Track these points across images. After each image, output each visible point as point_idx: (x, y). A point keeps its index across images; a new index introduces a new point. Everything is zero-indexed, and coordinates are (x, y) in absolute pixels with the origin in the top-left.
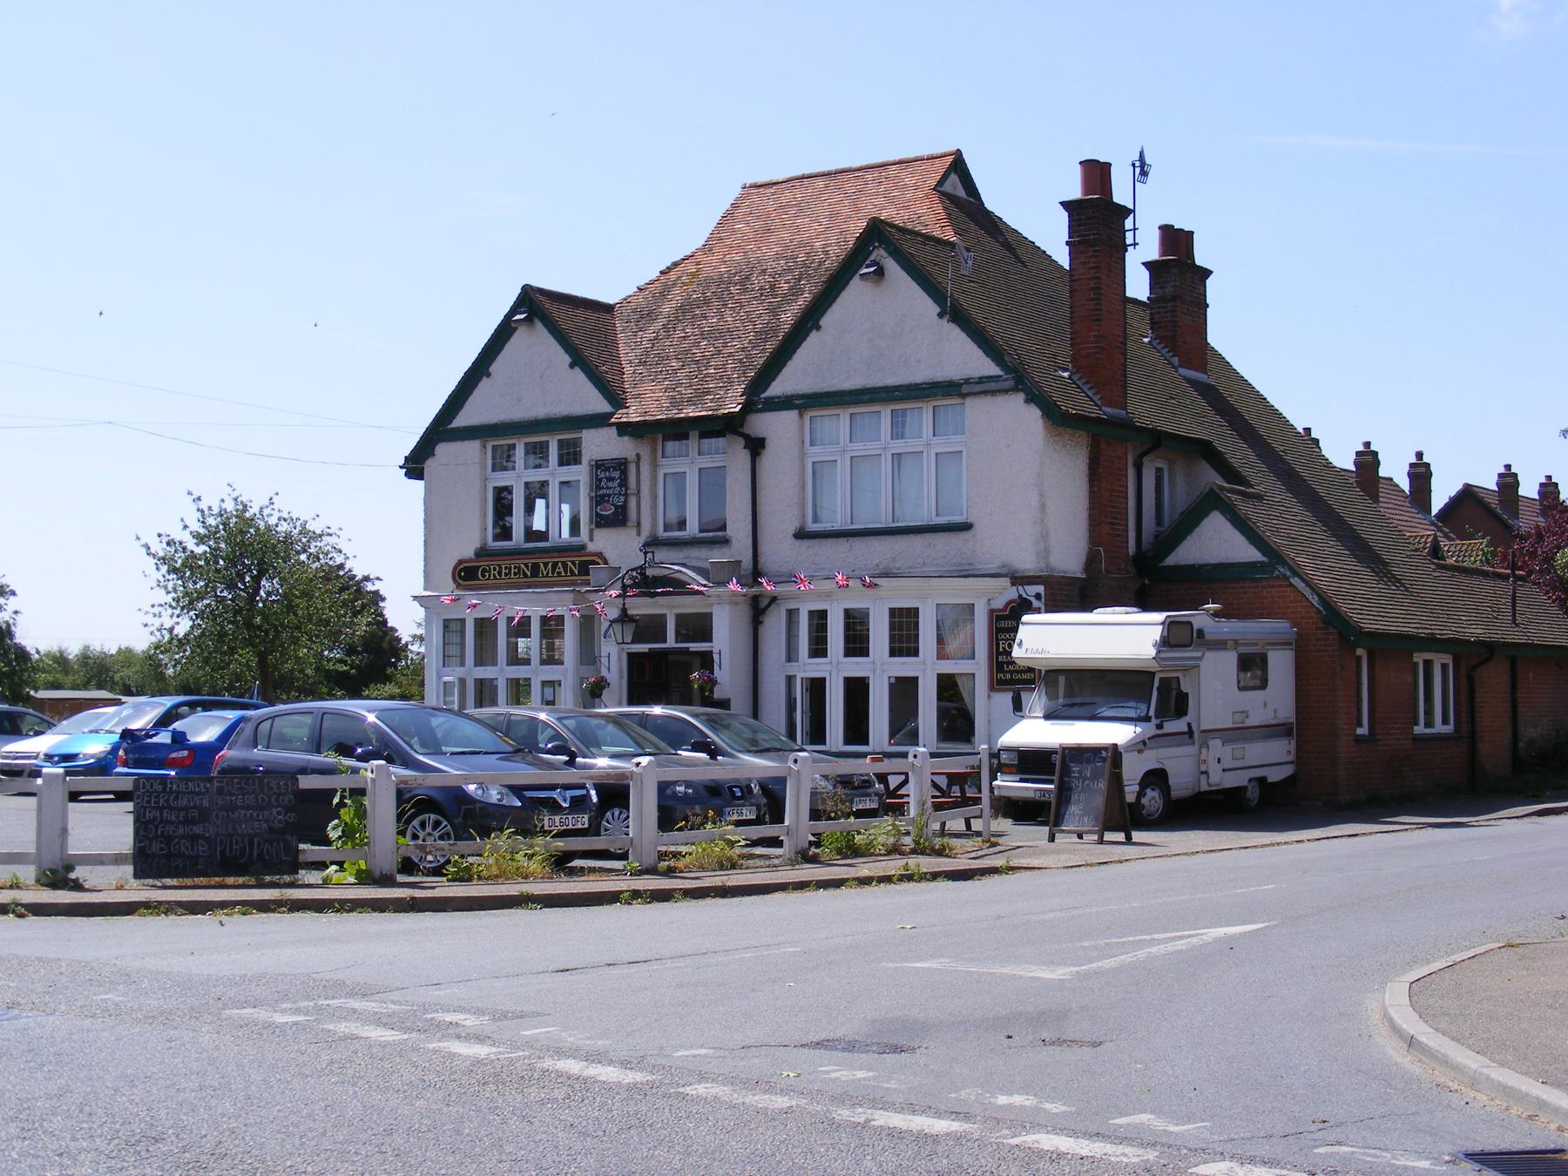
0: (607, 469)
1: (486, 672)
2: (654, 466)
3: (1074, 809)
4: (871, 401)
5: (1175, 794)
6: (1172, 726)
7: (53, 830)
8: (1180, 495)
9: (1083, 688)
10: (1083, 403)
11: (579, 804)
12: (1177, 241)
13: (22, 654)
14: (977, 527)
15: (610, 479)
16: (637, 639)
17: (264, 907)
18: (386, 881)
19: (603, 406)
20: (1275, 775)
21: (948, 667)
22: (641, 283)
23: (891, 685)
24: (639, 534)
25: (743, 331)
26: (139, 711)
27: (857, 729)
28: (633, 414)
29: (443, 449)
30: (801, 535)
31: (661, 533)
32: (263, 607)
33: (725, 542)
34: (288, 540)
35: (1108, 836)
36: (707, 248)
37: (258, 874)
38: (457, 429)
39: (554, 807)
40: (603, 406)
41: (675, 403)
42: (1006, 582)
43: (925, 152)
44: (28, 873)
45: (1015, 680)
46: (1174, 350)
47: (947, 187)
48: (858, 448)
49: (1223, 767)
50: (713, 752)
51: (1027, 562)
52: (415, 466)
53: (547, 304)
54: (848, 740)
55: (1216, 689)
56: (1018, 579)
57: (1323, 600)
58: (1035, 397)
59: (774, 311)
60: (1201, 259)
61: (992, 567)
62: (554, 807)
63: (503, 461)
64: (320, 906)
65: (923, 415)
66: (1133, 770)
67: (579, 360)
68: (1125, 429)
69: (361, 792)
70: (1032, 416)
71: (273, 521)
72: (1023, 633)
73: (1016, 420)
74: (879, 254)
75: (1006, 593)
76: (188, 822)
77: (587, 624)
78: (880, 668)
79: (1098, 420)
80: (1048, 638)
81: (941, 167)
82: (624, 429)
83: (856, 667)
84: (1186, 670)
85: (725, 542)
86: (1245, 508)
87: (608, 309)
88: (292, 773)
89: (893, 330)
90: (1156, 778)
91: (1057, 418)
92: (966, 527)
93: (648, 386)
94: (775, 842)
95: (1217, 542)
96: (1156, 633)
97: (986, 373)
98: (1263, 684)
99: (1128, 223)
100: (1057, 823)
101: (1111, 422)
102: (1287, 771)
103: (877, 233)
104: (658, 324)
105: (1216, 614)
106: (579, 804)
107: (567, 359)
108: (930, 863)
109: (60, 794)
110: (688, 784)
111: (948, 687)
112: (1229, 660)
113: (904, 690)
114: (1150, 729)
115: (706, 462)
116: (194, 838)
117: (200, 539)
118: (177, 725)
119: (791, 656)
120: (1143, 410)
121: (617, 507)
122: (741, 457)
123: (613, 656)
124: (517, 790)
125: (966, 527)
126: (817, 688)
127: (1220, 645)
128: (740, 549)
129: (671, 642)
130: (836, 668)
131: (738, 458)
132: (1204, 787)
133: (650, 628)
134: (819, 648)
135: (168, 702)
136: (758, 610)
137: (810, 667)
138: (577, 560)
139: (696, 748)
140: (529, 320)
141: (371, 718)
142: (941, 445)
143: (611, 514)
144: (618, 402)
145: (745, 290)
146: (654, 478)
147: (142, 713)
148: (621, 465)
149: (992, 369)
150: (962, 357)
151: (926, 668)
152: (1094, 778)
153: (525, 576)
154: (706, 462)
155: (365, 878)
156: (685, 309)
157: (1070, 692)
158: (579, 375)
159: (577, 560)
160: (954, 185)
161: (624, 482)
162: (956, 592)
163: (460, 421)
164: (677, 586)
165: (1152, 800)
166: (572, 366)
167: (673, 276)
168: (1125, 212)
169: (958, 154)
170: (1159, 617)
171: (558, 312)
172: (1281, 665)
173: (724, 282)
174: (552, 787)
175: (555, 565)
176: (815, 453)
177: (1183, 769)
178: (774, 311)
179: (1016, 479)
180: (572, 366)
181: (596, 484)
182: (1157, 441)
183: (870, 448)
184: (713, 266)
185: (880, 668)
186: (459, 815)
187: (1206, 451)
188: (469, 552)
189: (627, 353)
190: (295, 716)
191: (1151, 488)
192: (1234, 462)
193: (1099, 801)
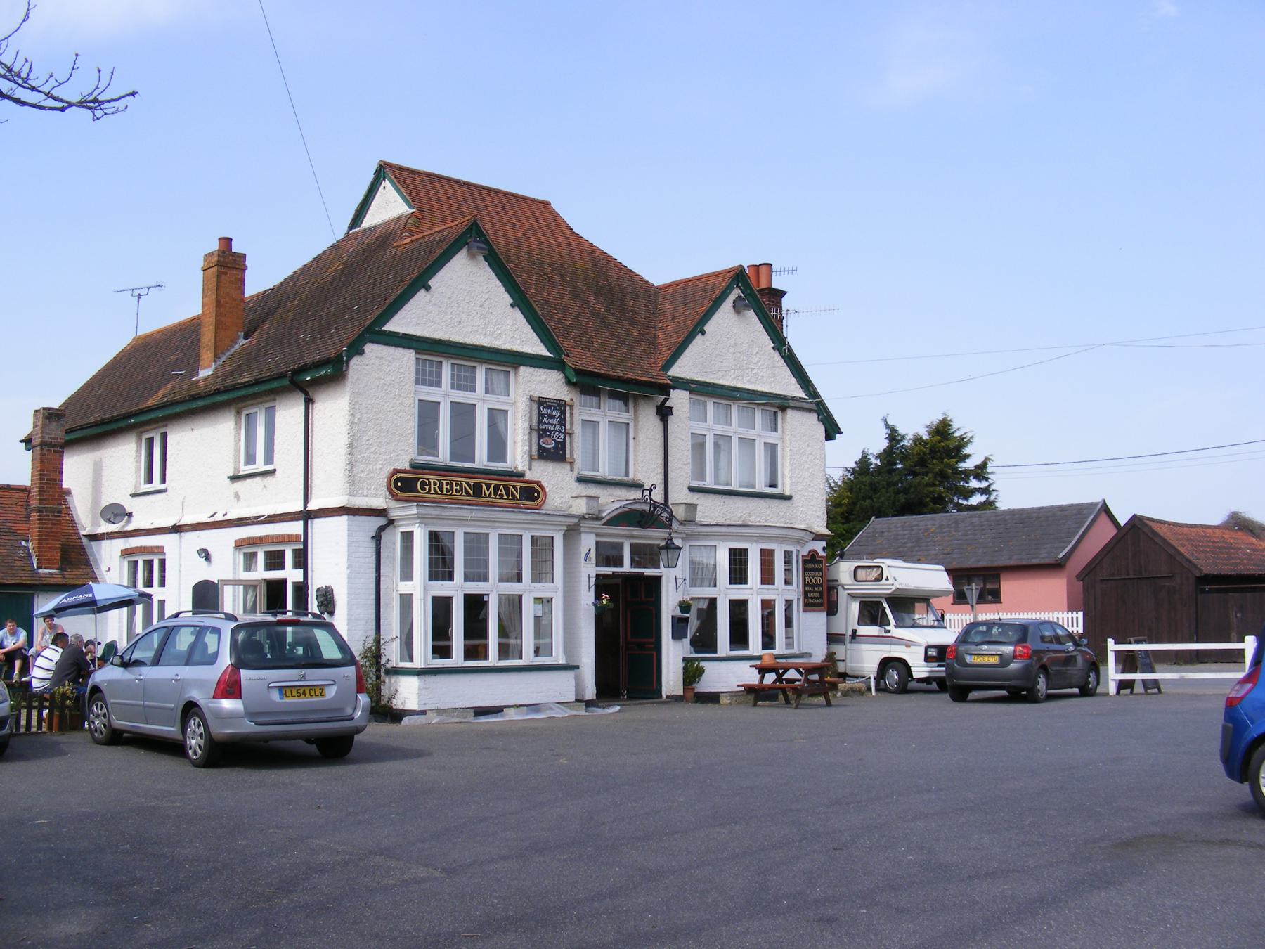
0: (549, 407)
14: (795, 498)
15: (551, 416)
23: (482, 596)
24: (572, 470)
38: (395, 335)
63: (427, 377)
92: (789, 498)
107: (699, 337)
121: (557, 443)
129: (627, 567)
130: (725, 593)
138: (519, 485)
148: (561, 406)
153: (468, 494)
158: (517, 315)
159: (519, 485)
166: (428, 288)
175: (497, 487)
180: (428, 288)
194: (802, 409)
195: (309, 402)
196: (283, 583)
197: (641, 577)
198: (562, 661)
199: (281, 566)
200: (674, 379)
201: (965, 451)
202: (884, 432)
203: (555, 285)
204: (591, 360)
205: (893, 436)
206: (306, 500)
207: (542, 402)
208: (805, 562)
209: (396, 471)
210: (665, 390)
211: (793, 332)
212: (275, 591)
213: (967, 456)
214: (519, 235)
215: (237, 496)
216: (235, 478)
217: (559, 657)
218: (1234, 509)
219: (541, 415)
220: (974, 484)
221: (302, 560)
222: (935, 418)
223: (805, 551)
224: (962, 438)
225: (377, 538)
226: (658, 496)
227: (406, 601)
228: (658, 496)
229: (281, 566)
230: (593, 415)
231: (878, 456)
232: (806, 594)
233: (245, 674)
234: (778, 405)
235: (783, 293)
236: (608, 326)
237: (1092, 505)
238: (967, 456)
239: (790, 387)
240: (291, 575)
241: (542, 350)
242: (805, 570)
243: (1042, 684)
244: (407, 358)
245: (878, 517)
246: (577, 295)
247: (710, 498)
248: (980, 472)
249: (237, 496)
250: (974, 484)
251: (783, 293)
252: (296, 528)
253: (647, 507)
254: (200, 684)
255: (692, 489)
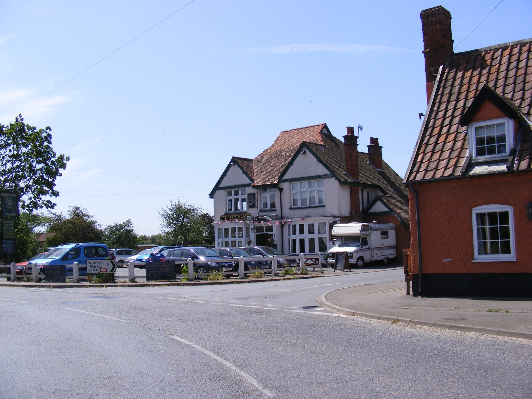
1: (227, 240)
2: (261, 194)
3: (339, 265)
4: (304, 180)
5: (366, 261)
6: (364, 247)
7: (131, 273)
8: (372, 197)
9: (347, 240)
10: (349, 180)
11: (230, 266)
12: (374, 141)
13: (135, 237)
16: (257, 232)
17: (168, 285)
18: (192, 280)
19: (250, 182)
20: (391, 257)
21: (321, 236)
22: (259, 154)
25: (279, 164)
26: (155, 250)
27: (312, 249)
28: (255, 184)
29: (217, 192)
30: (291, 208)
31: (262, 209)
32: (186, 227)
33: (275, 210)
34: (190, 210)
35: (345, 270)
36: (273, 146)
37: (168, 279)
39: (225, 266)
40: (250, 182)
41: (264, 181)
42: (332, 218)
43: (318, 124)
44: (127, 280)
45: (333, 238)
46: (374, 165)
47: (323, 131)
48: (302, 190)
49: (377, 256)
50: (264, 256)
51: (336, 213)
52: (211, 196)
53: (238, 161)
54: (310, 251)
55: (375, 239)
56: (335, 217)
57: (401, 219)
58: (337, 178)
59: (285, 160)
60: (380, 144)
61: (329, 215)
62: (225, 266)
63: (230, 194)
64: (178, 285)
65: (314, 183)
66: (356, 256)
67: (244, 172)
68: (358, 184)
69: (186, 264)
70: (337, 182)
71: (187, 206)
72: (334, 229)
73: (332, 184)
74: (305, 149)
75: (332, 220)
76: (156, 270)
77: (247, 229)
78: (307, 236)
79: (351, 182)
80: (340, 229)
81: (321, 127)
82: (254, 187)
83: (302, 236)
84: (368, 235)
85: (275, 210)
86: (385, 200)
87: (252, 160)
88: (174, 261)
89: (308, 164)
90: (361, 258)
91: (342, 183)
92: (324, 206)
93: (259, 178)
94: (270, 273)
95: (379, 207)
96: (360, 228)
97: (325, 174)
98: (387, 238)
99: (358, 140)
100: (336, 268)
101: (354, 183)
102: (395, 256)
103: (304, 144)
104: (262, 164)
105: (376, 223)
106: (230, 266)
108: (305, 275)
109: (133, 266)
110: (254, 262)
111: (321, 241)
112: (379, 233)
113: (312, 241)
114: (360, 248)
115: (271, 193)
116: (157, 273)
117: (171, 211)
118: (162, 253)
119: (289, 234)
120: (362, 179)
122: (278, 192)
123: (253, 236)
124: (218, 263)
125: (324, 206)
126: (294, 241)
127: (376, 230)
128: (278, 212)
129: (265, 232)
131: (277, 193)
132: (373, 260)
133: (259, 229)
134: (294, 233)
135: (161, 247)
136: (282, 226)
137: (293, 237)
139: (260, 255)
140: (234, 164)
141: (192, 251)
142: (319, 189)
143: (251, 205)
144: (253, 181)
145: (280, 156)
146: (261, 197)
147: (155, 251)
148: (254, 195)
149: (328, 173)
150: (322, 170)
151: (316, 236)
152: (343, 258)
154: (271, 193)
155: (188, 280)
156: (268, 160)
157: (345, 241)
158: (244, 176)
160: (325, 131)
161: (254, 198)
162: (322, 220)
163: (221, 186)
164: (266, 220)
165: (360, 263)
167: (265, 153)
168: (357, 137)
169: (325, 124)
170: (361, 224)
171: (240, 162)
172: (392, 234)
173: (276, 154)
174: (225, 263)
176: (293, 191)
177: (367, 257)
178: (285, 160)
179: (334, 196)
181: (249, 199)
182: (366, 186)
183: (304, 190)
184: (274, 150)
185: (307, 236)
186: (206, 268)
187: (378, 187)
188: (223, 214)
189: (255, 170)
190: (179, 250)
191: (363, 197)
192: (385, 189)
193: (343, 263)
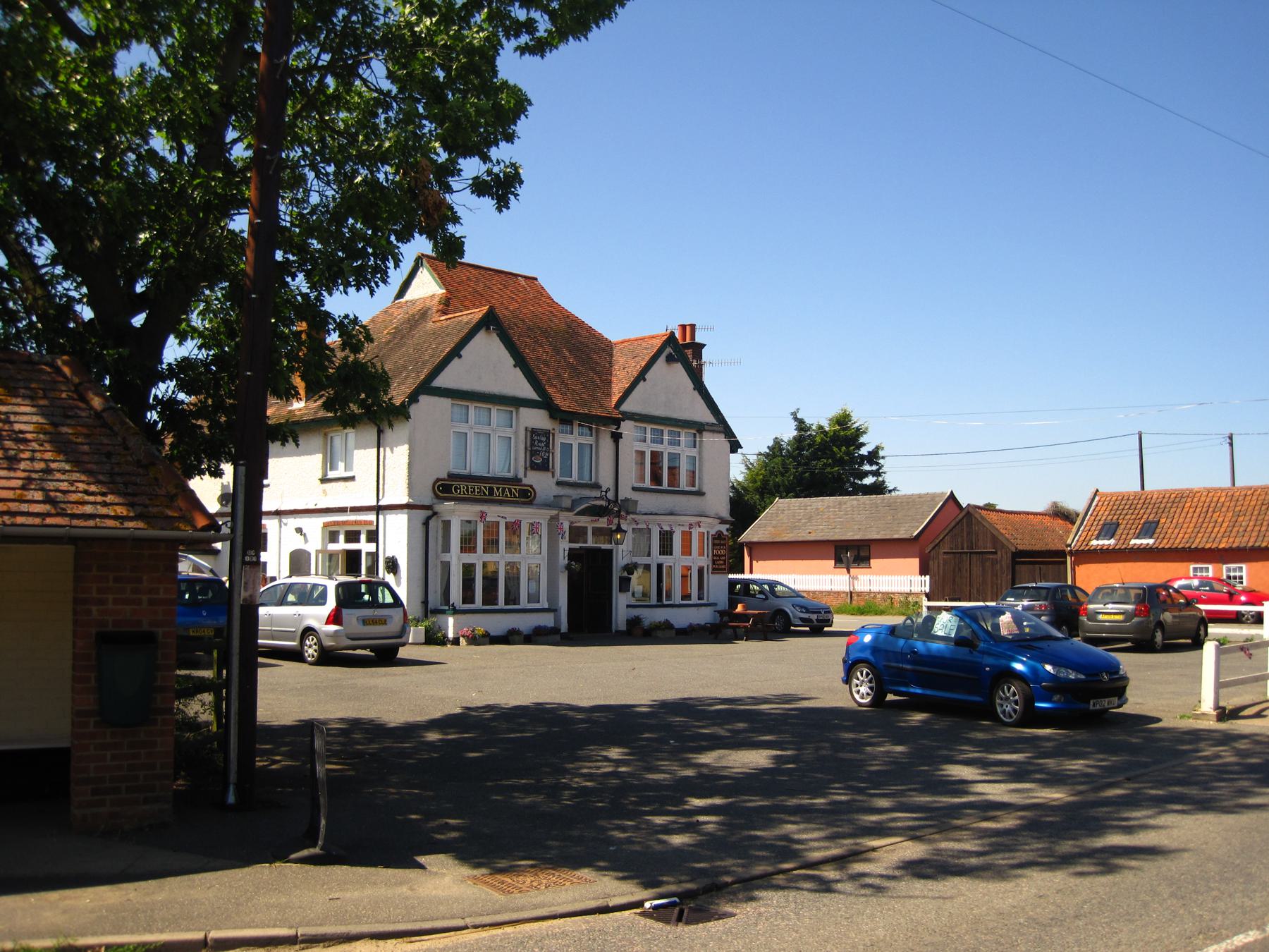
15: (540, 441)
129: (590, 543)
148: (546, 433)
166: (460, 357)
175: (504, 490)
180: (460, 357)
194: (713, 431)
195: (380, 432)
196: (358, 552)
197: (599, 550)
198: (546, 606)
199: (358, 541)
200: (624, 413)
201: (862, 440)
202: (793, 424)
203: (542, 345)
204: (567, 402)
205: (801, 425)
206: (378, 500)
207: (534, 432)
208: (714, 539)
209: (438, 480)
210: (617, 422)
211: (709, 380)
212: (352, 560)
213: (863, 445)
214: (516, 306)
215: (324, 491)
216: (324, 480)
217: (544, 604)
218: (1054, 500)
219: (533, 440)
220: (867, 467)
221: (373, 537)
222: (834, 411)
223: (713, 532)
224: (858, 429)
225: (426, 524)
226: (611, 495)
227: (446, 566)
228: (611, 495)
229: (358, 541)
230: (567, 439)
231: (789, 443)
232: (714, 562)
233: (345, 611)
234: (700, 428)
235: (703, 346)
236: (579, 375)
237: (933, 497)
238: (863, 445)
239: (708, 418)
240: (365, 547)
241: (532, 395)
242: (714, 545)
243: (1159, 636)
244: (446, 403)
245: (781, 497)
246: (557, 352)
247: (648, 495)
248: (873, 457)
249: (324, 491)
250: (867, 467)
251: (703, 346)
252: (371, 517)
253: (603, 503)
254: (317, 618)
255: (634, 489)
